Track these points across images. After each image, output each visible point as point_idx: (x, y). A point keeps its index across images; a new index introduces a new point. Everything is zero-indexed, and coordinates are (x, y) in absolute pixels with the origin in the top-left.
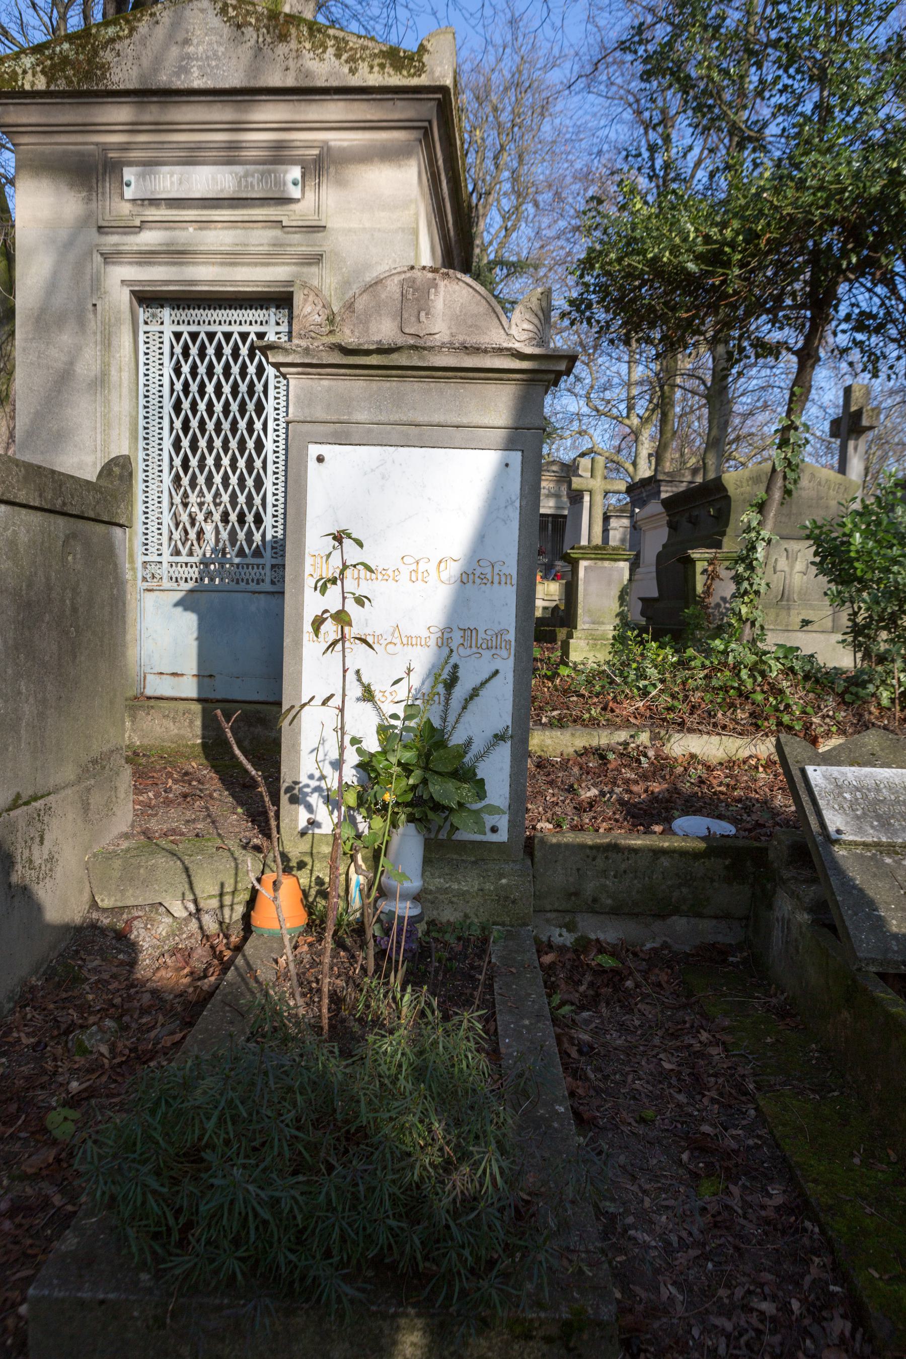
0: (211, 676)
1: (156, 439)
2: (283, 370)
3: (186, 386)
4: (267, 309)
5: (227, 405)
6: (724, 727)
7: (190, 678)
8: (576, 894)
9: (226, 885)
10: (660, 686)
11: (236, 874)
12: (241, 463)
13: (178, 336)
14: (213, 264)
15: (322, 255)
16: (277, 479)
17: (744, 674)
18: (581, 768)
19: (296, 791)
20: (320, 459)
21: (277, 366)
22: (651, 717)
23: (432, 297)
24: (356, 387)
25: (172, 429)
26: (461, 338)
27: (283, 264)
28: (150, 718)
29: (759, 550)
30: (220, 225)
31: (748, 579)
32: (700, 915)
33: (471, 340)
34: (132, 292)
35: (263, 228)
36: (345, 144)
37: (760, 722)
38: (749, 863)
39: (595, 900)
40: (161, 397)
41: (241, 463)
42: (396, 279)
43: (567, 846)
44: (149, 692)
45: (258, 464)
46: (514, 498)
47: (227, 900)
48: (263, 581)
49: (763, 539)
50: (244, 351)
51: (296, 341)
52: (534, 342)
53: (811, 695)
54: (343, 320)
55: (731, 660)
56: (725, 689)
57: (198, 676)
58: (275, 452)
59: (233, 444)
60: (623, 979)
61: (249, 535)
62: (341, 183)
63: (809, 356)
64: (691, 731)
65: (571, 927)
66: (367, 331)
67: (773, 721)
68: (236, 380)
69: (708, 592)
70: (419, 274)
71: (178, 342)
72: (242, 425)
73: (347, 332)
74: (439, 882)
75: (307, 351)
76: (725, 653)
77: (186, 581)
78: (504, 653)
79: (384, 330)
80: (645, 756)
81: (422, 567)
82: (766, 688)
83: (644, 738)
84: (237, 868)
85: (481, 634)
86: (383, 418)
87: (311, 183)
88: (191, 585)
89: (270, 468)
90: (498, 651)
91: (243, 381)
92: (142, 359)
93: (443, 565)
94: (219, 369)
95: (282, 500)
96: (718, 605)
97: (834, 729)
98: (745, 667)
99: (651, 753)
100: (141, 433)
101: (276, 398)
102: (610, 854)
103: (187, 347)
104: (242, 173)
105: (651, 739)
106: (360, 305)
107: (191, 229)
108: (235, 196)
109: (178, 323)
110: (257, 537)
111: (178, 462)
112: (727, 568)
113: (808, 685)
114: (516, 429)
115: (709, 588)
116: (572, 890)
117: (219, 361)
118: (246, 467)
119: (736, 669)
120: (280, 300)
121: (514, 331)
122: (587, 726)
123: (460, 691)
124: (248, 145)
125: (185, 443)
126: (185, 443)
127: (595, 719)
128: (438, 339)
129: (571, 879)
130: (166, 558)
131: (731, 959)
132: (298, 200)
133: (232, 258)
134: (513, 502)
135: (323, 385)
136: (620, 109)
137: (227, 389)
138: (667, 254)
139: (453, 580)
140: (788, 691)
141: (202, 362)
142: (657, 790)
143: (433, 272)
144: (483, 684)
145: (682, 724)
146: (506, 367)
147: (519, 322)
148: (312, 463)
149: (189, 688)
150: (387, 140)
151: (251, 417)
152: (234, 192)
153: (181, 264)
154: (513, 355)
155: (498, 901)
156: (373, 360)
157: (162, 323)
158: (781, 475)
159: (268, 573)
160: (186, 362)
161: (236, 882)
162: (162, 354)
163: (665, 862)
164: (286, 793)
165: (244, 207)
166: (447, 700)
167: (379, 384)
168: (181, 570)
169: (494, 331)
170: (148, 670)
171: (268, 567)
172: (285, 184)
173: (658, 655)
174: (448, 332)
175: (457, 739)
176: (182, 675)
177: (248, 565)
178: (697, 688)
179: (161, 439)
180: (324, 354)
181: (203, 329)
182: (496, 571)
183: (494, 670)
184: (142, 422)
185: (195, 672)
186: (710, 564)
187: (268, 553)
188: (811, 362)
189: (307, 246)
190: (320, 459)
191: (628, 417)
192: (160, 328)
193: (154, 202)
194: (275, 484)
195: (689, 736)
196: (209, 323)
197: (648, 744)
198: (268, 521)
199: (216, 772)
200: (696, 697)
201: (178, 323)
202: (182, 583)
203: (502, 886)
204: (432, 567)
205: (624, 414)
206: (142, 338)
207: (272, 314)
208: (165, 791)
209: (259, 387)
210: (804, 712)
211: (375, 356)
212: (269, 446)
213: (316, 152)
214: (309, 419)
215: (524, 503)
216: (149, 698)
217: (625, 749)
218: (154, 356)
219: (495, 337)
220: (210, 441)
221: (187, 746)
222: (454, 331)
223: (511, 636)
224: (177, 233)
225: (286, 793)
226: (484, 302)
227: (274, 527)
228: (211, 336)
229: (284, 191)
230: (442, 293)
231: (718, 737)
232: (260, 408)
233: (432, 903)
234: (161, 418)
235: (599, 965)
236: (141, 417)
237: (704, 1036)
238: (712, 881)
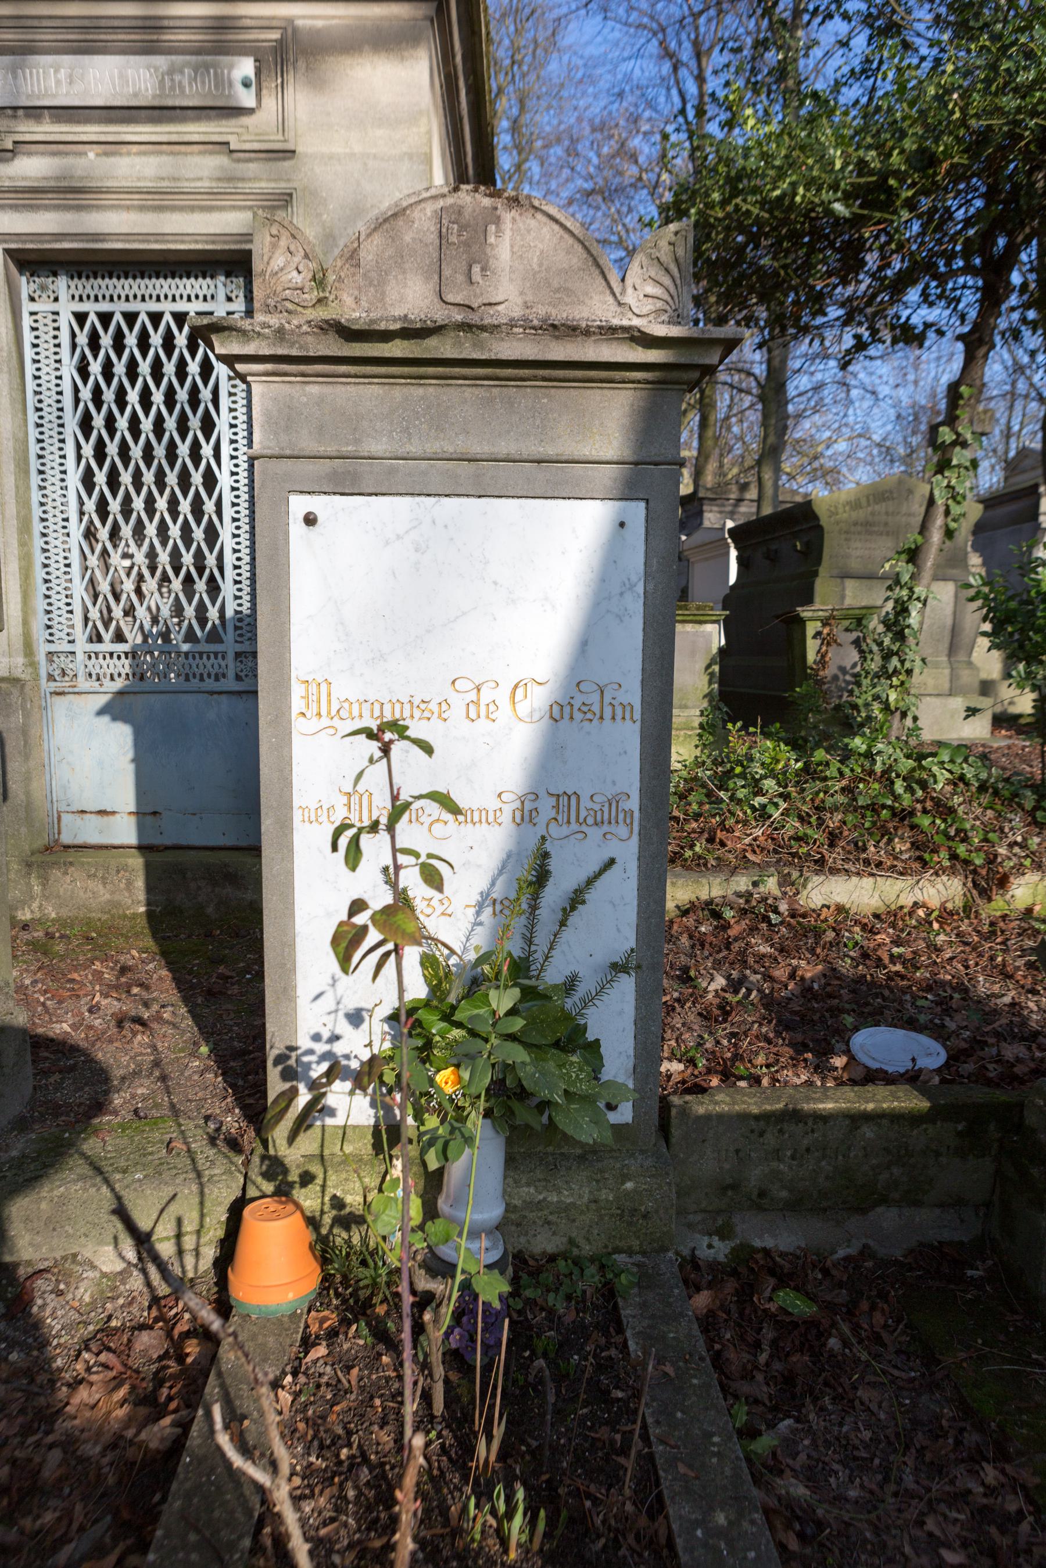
0: (155, 813)
1: (56, 472)
2: (240, 367)
3: (97, 393)
5: (159, 421)
6: (879, 865)
7: (126, 817)
8: (734, 1187)
9: (186, 1222)
10: (783, 805)
11: (202, 1203)
12: (185, 506)
13: (81, 318)
14: (128, 208)
15: (290, 195)
16: (238, 528)
17: (899, 787)
18: (691, 937)
19: (292, 1062)
20: (310, 520)
21: (229, 360)
22: (775, 851)
23: (492, 239)
24: (364, 396)
25: (79, 457)
26: (542, 310)
27: (234, 208)
28: (68, 879)
29: (914, 614)
30: (135, 148)
31: (897, 654)
32: (917, 1204)
33: (560, 314)
34: (7, 251)
35: (200, 153)
36: (319, 24)
37: (927, 856)
38: (992, 1127)
39: (762, 1194)
40: (61, 410)
41: (185, 506)
42: (430, 208)
43: (720, 1117)
44: (66, 839)
45: (209, 506)
46: (634, 578)
47: (189, 1242)
48: (224, 676)
49: (918, 599)
50: (181, 340)
51: (259, 317)
52: (665, 317)
53: (990, 813)
54: (340, 279)
55: (878, 768)
56: (874, 808)
57: (137, 813)
58: (234, 489)
59: (172, 478)
60: (823, 1335)
61: (201, 611)
62: (318, 84)
63: (981, 342)
64: (834, 871)
65: (724, 1233)
67: (944, 854)
68: (170, 384)
69: (822, 662)
70: (468, 199)
71: (82, 327)
72: (183, 450)
73: (348, 300)
74: (527, 1192)
75: (280, 333)
76: (869, 755)
77: (112, 679)
78: (622, 831)
79: (411, 298)
80: (776, 911)
81: (486, 696)
82: (929, 805)
83: (771, 885)
84: (202, 1194)
85: (585, 802)
87: (270, 85)
88: (119, 684)
89: (228, 512)
90: (613, 828)
91: (182, 386)
92: (29, 353)
93: (520, 692)
94: (145, 367)
95: (247, 559)
96: (835, 678)
97: (1027, 862)
98: (898, 776)
99: (783, 907)
100: (34, 464)
101: (231, 410)
102: (785, 1126)
103: (95, 333)
104: (165, 68)
105: (780, 885)
106: (368, 253)
107: (91, 155)
108: (156, 103)
109: (81, 299)
110: (213, 613)
111: (90, 505)
112: (847, 630)
113: (985, 799)
114: (636, 464)
115: (823, 656)
116: (729, 1181)
117: (144, 356)
118: (193, 512)
119: (886, 778)
120: (233, 263)
121: (630, 298)
122: (688, 868)
123: (554, 895)
124: (172, 23)
125: (101, 478)
126: (101, 478)
127: (700, 857)
128: (503, 313)
129: (727, 1166)
130: (82, 646)
131: (970, 1273)
132: (250, 111)
133: (159, 198)
134: (632, 587)
136: (643, 40)
137: (158, 397)
138: (801, 190)
139: (536, 717)
140: (961, 810)
141: (120, 358)
142: (808, 975)
144: (590, 882)
145: (821, 862)
146: (620, 359)
147: (638, 282)
148: (296, 528)
149: (125, 831)
150: (382, 18)
151: (195, 437)
152: (154, 97)
153: (79, 208)
154: (633, 339)
155: (622, 1216)
156: (396, 349)
157: (56, 299)
158: (942, 509)
159: (231, 665)
160: (95, 357)
161: (202, 1216)
162: (58, 346)
163: (868, 1132)
164: (275, 1064)
165: (171, 120)
166: (534, 908)
168: (104, 664)
169: (596, 298)
170: (63, 807)
171: (231, 656)
172: (231, 84)
173: (766, 751)
175: (553, 975)
176: (113, 813)
177: (201, 654)
178: (837, 809)
179: (64, 472)
181: (118, 308)
182: (607, 699)
183: (606, 856)
184: (34, 449)
185: (133, 809)
186: (824, 625)
187: (230, 636)
188: (982, 351)
189: (269, 180)
190: (310, 520)
192: (54, 307)
193: (34, 112)
194: (235, 536)
195: (833, 879)
196: (127, 299)
197: (777, 892)
198: (228, 589)
199: (171, 965)
200: (833, 821)
201: (81, 299)
202: (106, 681)
203: (627, 1193)
204: (502, 696)
206: (27, 322)
207: (220, 285)
208: (90, 1011)
209: (206, 394)
210: (986, 840)
211: (398, 342)
212: (225, 481)
213: (276, 35)
214: (288, 452)
215: (651, 587)
216: (67, 847)
217: (747, 902)
218: (47, 349)
219: (598, 308)
220: (137, 476)
221: (125, 916)
222: (529, 298)
223: (634, 804)
224: (70, 161)
225: (275, 1064)
226: (579, 248)
227: (236, 598)
228: (131, 318)
229: (230, 96)
230: (508, 234)
231: (871, 879)
232: (208, 425)
233: (518, 1225)
234: (62, 441)
235: (783, 1310)
236: (32, 440)
237: (990, 1474)
238: (938, 1154)
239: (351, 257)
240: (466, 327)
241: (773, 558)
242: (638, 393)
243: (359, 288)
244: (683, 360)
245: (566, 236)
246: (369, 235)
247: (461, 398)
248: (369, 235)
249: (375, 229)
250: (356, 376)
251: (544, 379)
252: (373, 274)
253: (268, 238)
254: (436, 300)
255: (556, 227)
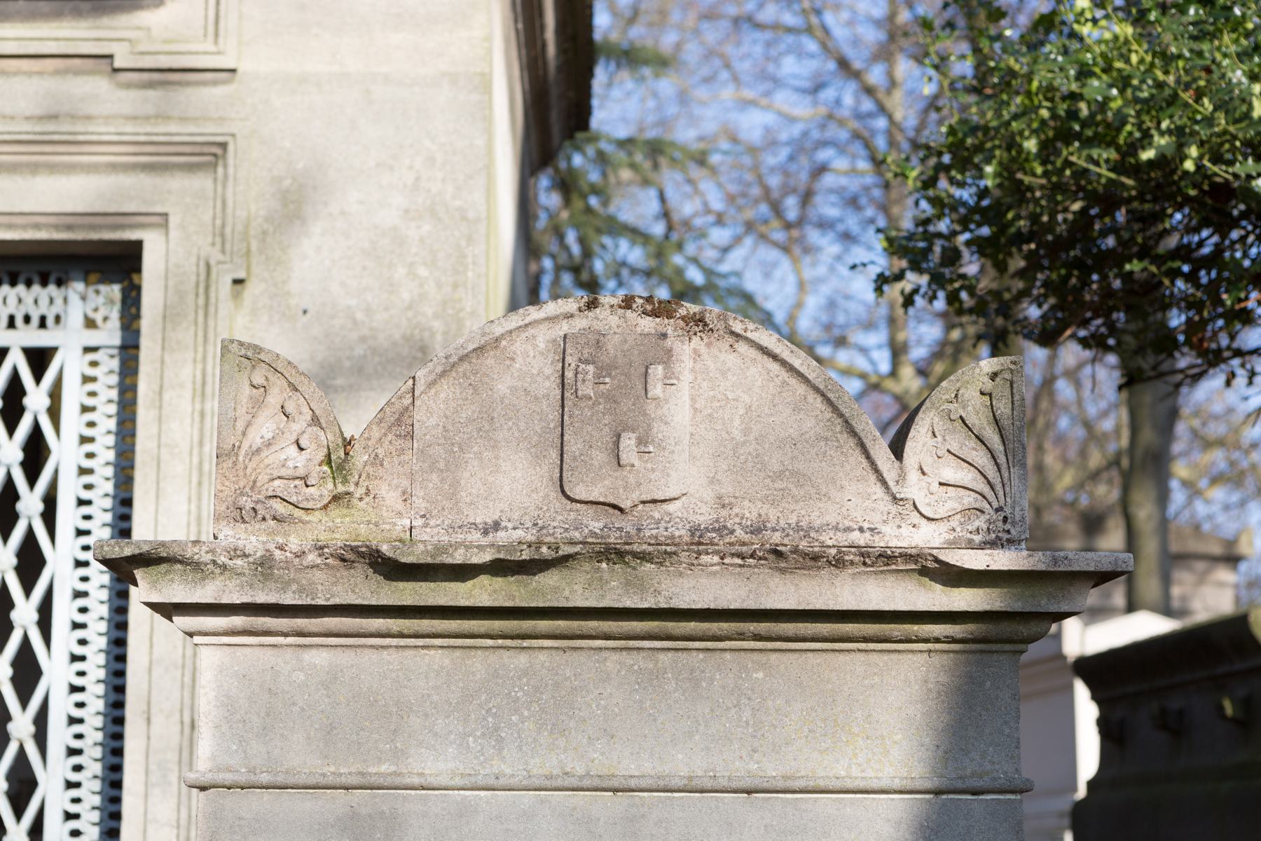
4: (60, 283)
15: (224, 145)
16: (78, 768)
23: (656, 390)
26: (750, 511)
35: (57, 72)
54: (376, 461)
66: (453, 496)
70: (614, 320)
73: (390, 496)
75: (264, 567)
79: (505, 496)
86: (509, 766)
89: (59, 735)
114: (937, 792)
121: (914, 488)
135: (311, 663)
143: (655, 314)
154: (924, 572)
167: (493, 657)
174: (709, 495)
180: (318, 575)
191: (894, 373)
205: (885, 367)
211: (484, 579)
214: (265, 778)
219: (852, 506)
222: (727, 489)
226: (818, 402)
230: (687, 377)
239: (398, 422)
240: (614, 554)
241: (1174, 726)
242: (936, 659)
243: (412, 476)
244: (1018, 606)
245: (793, 381)
246: (431, 384)
247: (601, 674)
248: (431, 384)
249: (443, 374)
250: (401, 635)
251: (758, 637)
252: (437, 451)
253: (247, 390)
254: (555, 494)
255: (775, 367)
